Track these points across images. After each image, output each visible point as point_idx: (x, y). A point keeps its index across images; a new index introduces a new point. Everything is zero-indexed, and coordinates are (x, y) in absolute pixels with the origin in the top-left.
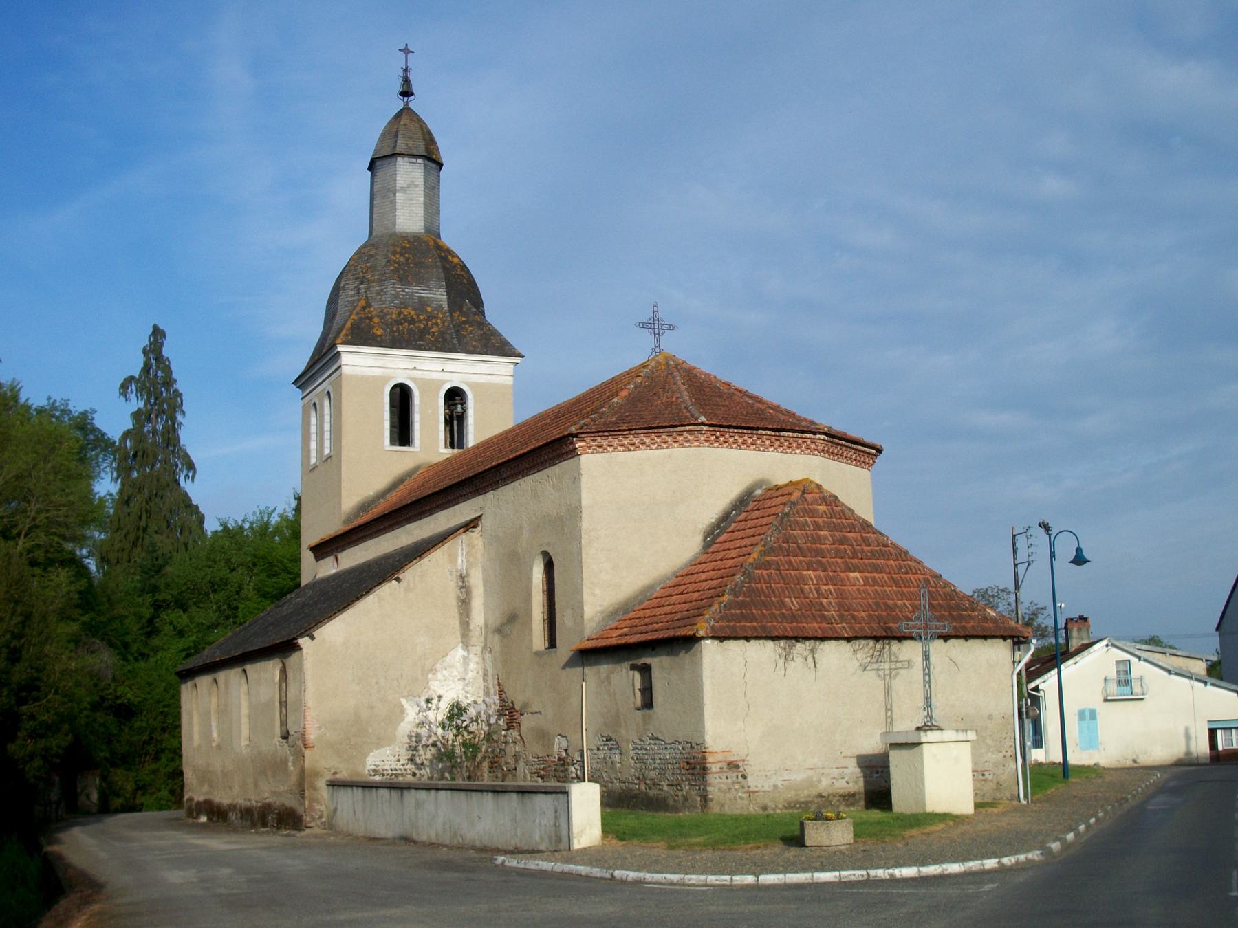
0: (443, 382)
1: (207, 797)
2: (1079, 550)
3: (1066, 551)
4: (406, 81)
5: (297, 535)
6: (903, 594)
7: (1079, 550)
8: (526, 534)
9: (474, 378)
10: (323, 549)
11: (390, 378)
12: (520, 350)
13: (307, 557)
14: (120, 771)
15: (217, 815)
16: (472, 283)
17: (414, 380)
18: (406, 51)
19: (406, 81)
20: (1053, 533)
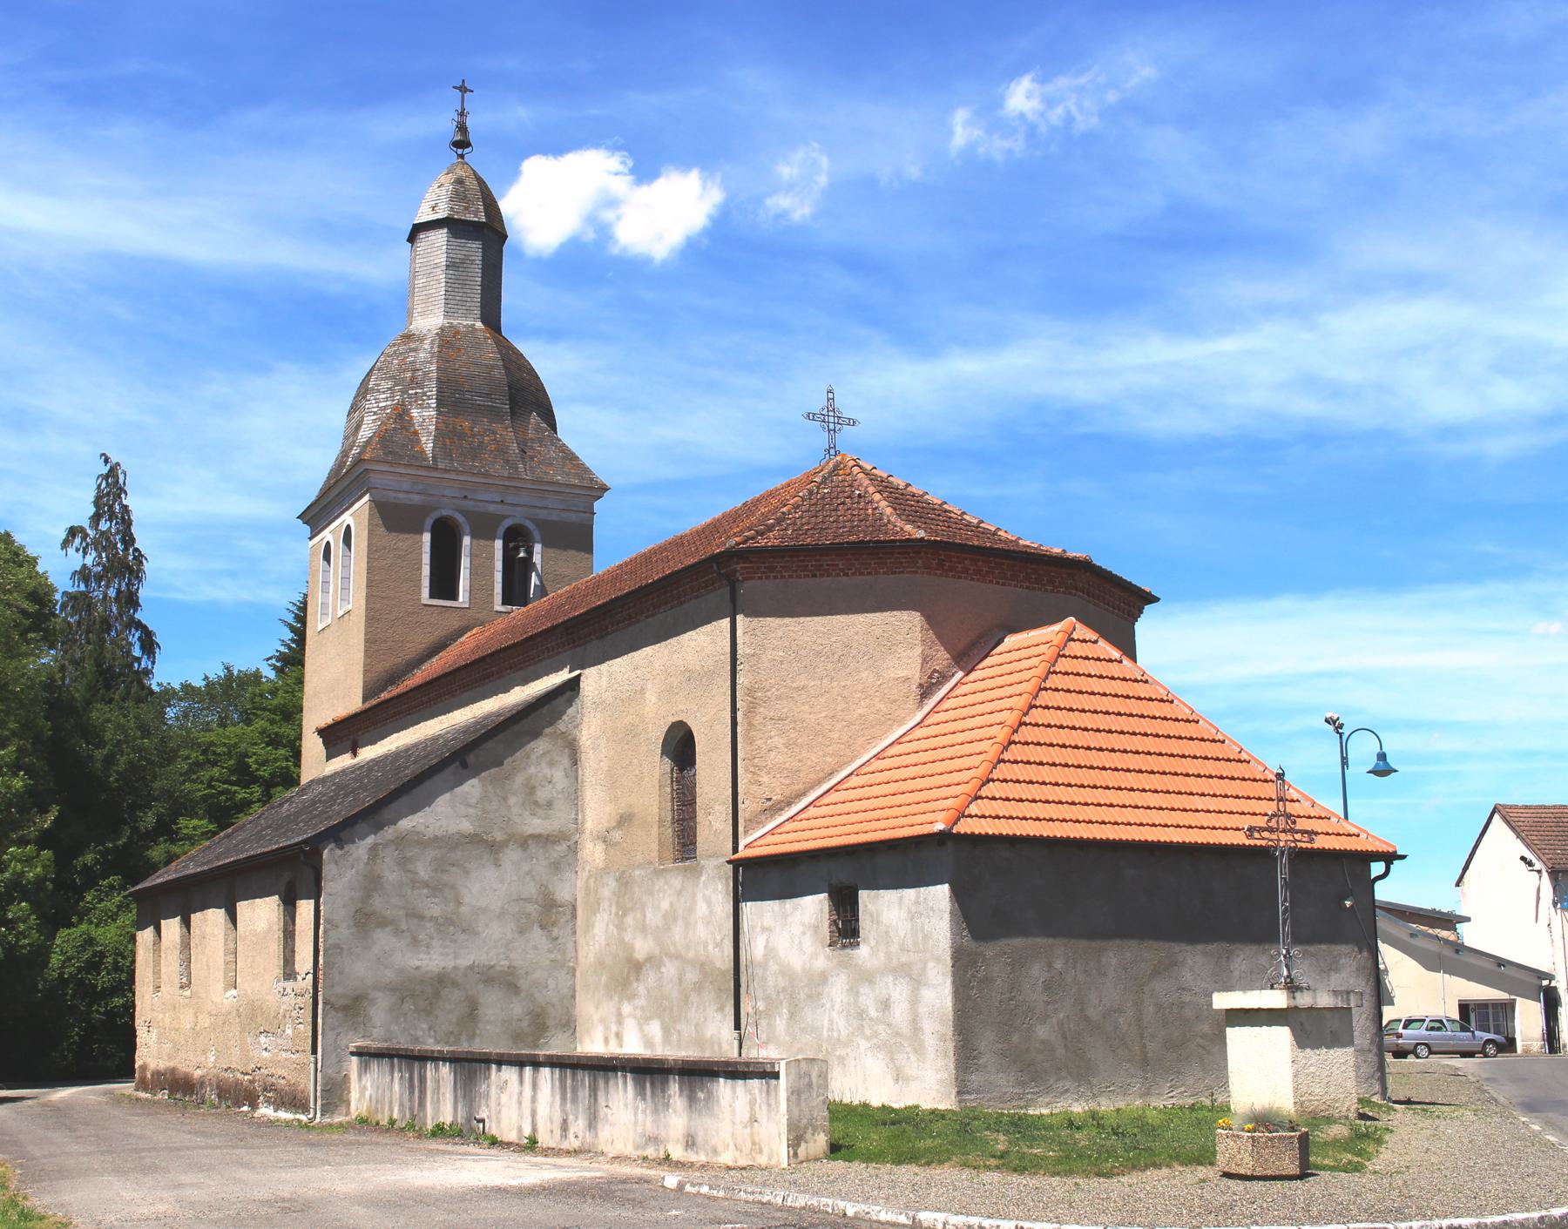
0: (505, 517)
1: (171, 1064)
2: (1382, 756)
3: (1363, 751)
4: (462, 128)
5: (292, 713)
6: (1549, 1167)
7: (1382, 756)
8: (651, 697)
9: (543, 514)
10: (340, 736)
11: (432, 509)
12: (1463, 913)
13: (312, 746)
14: (539, 793)
15: (180, 1086)
16: (540, 389)
17: (464, 513)
18: (463, 89)
19: (462, 128)
20: (1346, 731)
